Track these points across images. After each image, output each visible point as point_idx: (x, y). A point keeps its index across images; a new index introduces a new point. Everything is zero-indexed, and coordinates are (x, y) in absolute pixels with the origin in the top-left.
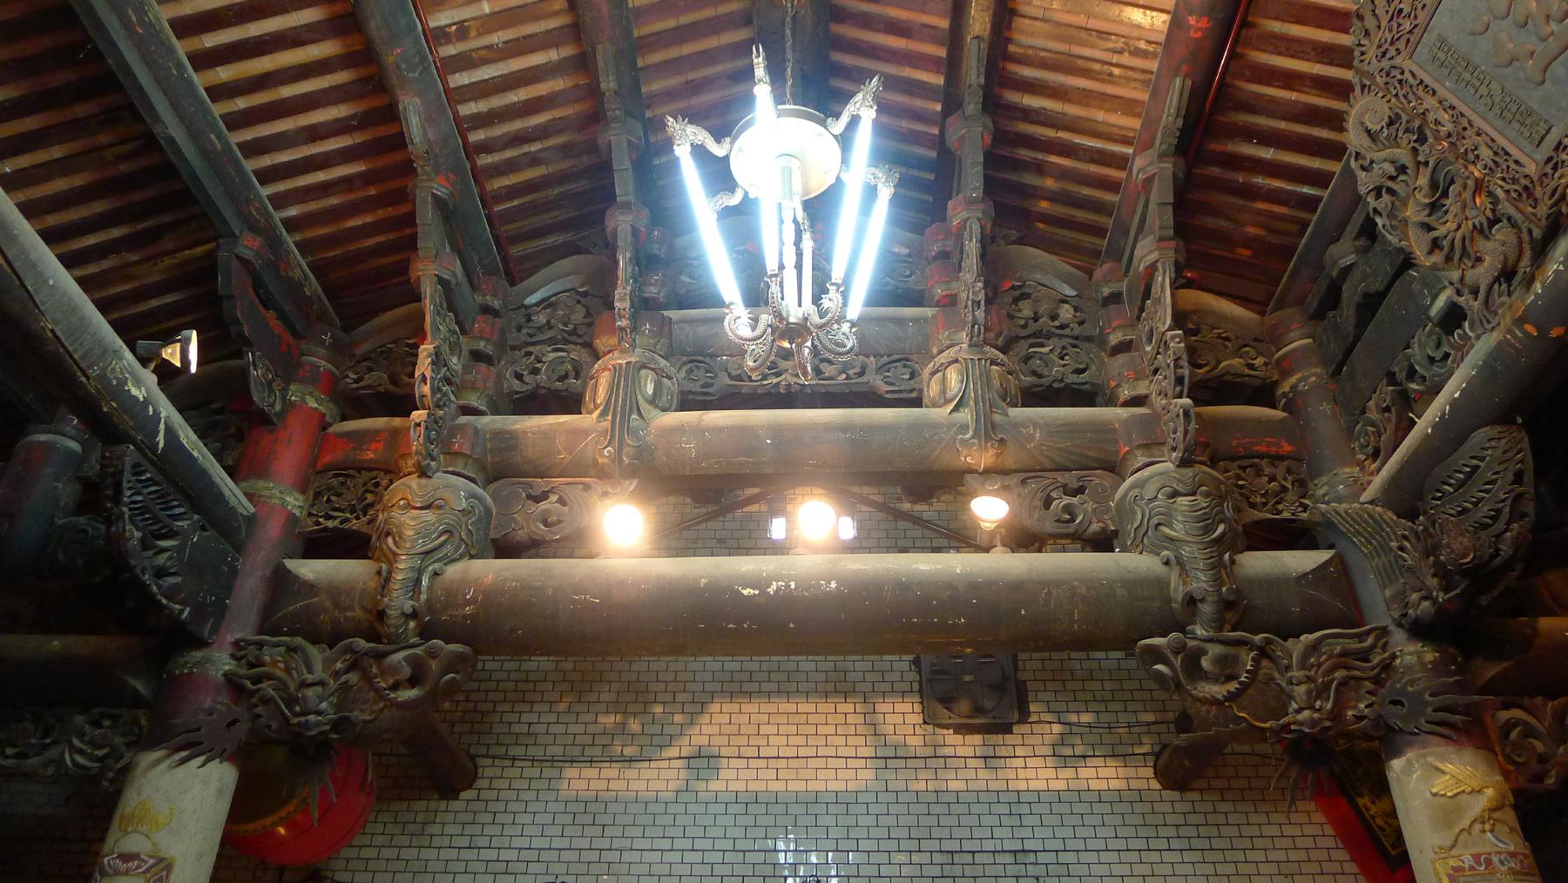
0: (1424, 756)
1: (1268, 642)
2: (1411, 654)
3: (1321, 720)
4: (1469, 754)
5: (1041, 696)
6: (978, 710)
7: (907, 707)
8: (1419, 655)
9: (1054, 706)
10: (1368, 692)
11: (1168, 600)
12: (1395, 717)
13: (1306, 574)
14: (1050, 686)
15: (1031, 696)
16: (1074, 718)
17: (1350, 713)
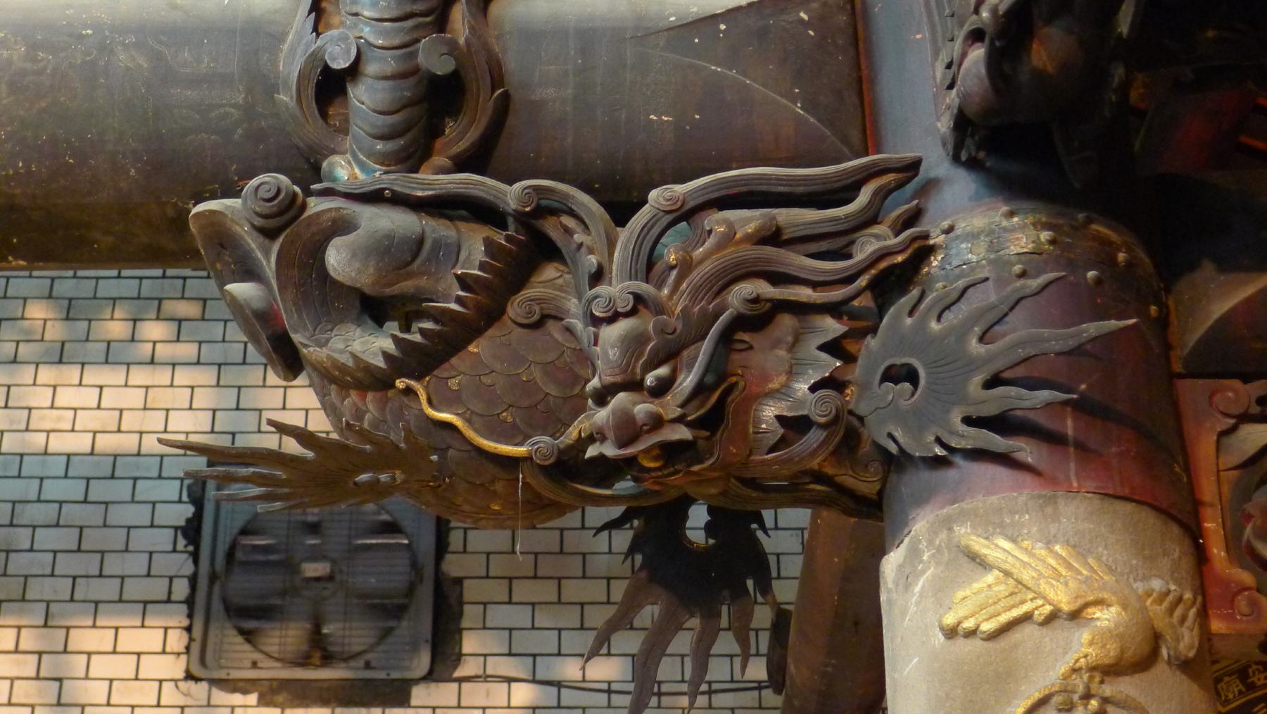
0: (948, 523)
1: (545, 208)
2: (972, 236)
3: (657, 422)
4: (1077, 512)
5: (499, 615)
6: (320, 649)
7: (150, 639)
8: (995, 239)
9: (525, 641)
10: (827, 348)
11: (267, 86)
12: (891, 420)
13: (714, 18)
14: (523, 591)
15: (471, 614)
16: (570, 670)
17: (769, 411)
